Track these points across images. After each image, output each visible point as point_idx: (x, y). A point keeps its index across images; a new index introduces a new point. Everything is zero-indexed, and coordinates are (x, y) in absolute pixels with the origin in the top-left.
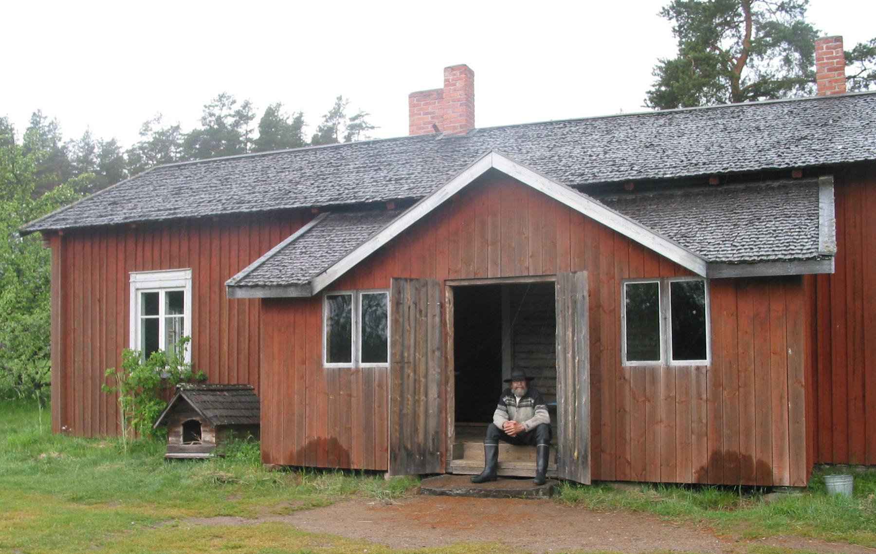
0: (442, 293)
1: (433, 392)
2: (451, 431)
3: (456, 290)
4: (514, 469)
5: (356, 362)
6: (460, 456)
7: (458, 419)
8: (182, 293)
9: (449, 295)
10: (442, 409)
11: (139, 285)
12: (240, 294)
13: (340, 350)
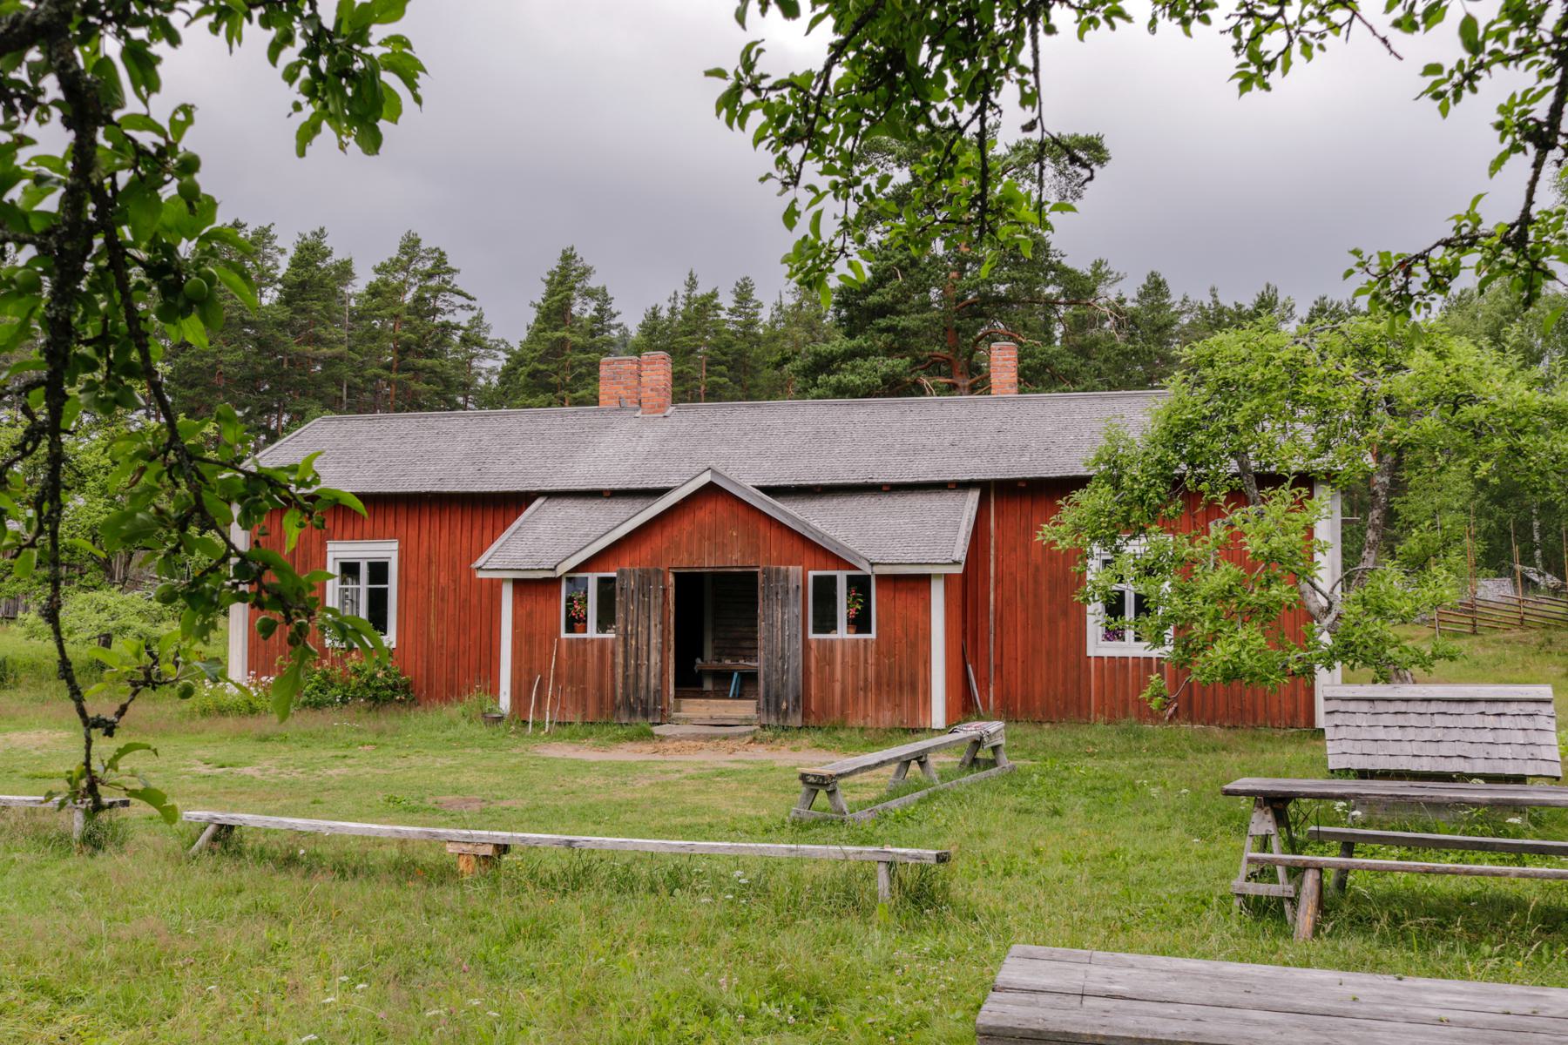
0: (665, 578)
1: (655, 657)
2: (672, 692)
3: (676, 575)
4: (796, 687)
5: (842, 633)
6: (678, 710)
7: (677, 685)
8: (386, 564)
9: (671, 579)
10: (663, 673)
11: (338, 555)
12: (480, 575)
13: (575, 622)
